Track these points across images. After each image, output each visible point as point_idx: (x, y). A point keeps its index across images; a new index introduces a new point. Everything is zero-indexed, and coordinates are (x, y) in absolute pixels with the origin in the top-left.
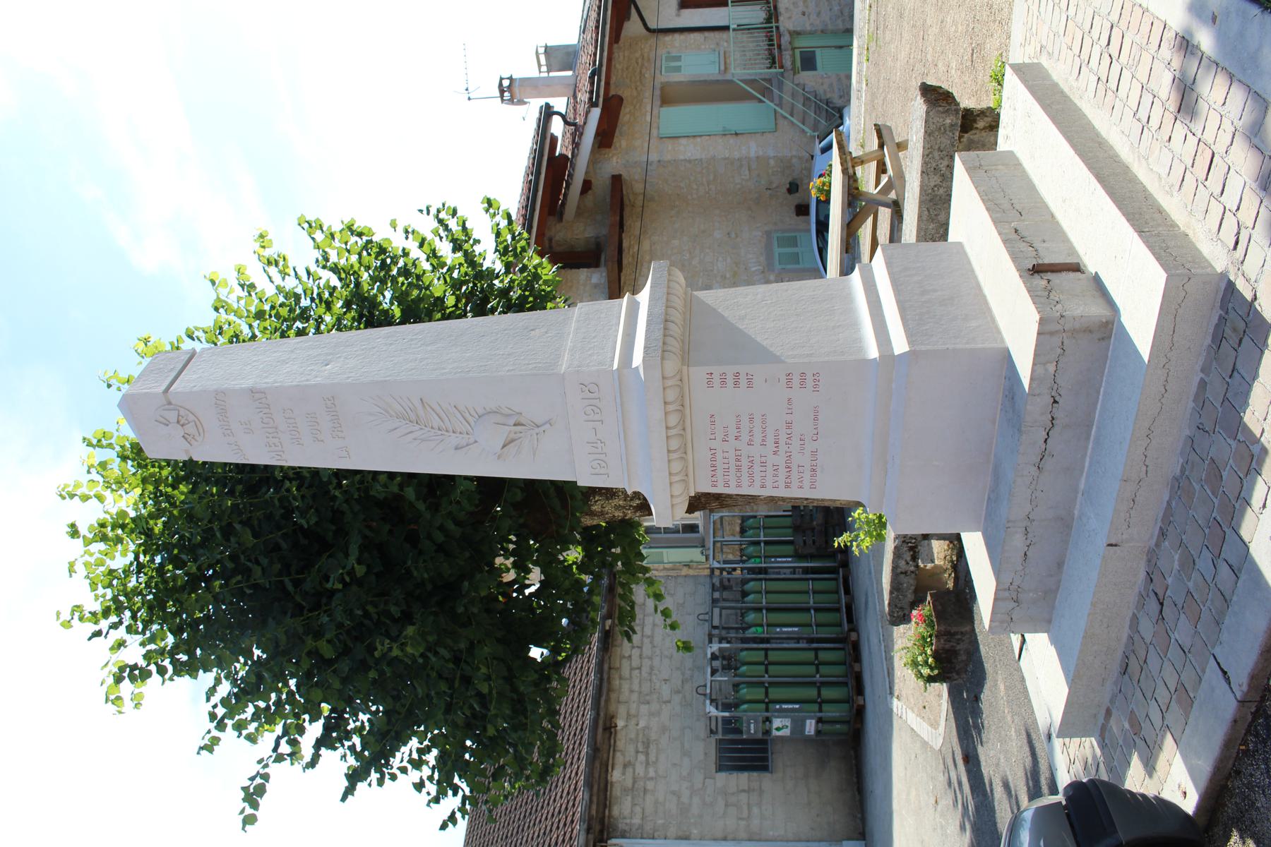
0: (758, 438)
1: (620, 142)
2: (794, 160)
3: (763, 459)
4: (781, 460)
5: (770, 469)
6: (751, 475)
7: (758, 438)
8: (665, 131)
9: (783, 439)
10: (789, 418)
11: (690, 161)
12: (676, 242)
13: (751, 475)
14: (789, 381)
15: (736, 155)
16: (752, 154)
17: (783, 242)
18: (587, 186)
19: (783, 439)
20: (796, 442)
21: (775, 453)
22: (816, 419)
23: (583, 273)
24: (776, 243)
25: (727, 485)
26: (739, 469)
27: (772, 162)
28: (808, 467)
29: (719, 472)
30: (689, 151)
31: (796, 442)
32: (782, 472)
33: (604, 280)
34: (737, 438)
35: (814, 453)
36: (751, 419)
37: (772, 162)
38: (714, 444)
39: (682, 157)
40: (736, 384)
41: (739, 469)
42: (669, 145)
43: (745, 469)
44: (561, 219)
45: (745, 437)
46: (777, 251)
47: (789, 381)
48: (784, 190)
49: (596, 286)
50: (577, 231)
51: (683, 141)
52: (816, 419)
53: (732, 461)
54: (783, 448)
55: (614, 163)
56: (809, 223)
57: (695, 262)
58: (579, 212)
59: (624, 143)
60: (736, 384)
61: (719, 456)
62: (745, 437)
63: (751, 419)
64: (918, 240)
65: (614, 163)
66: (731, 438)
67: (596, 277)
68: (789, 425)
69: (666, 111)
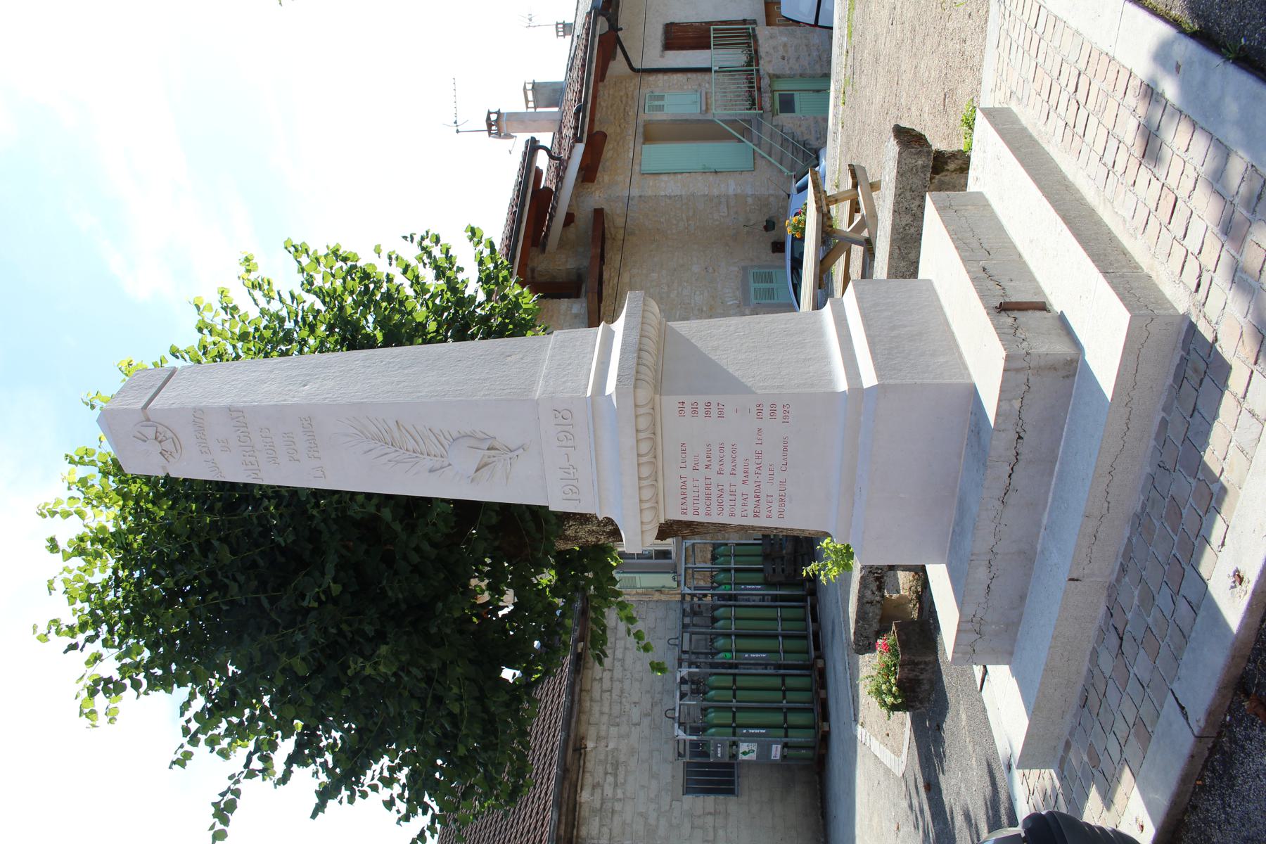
0: (727, 468)
1: (603, 177)
2: (771, 199)
3: (733, 488)
4: (750, 489)
5: (739, 498)
6: (720, 504)
7: (727, 468)
8: (646, 167)
9: (752, 468)
10: (759, 448)
11: (670, 197)
12: (655, 275)
13: (720, 504)
14: (759, 412)
15: (716, 192)
16: (731, 192)
17: (760, 278)
18: (570, 218)
19: (752, 468)
20: (765, 472)
21: (745, 482)
22: (785, 449)
23: (564, 303)
24: (752, 280)
25: (696, 512)
26: (708, 497)
27: (750, 200)
28: (776, 497)
29: (690, 501)
30: (670, 187)
31: (765, 472)
32: (751, 503)
33: (583, 311)
34: (707, 467)
35: (783, 483)
36: (722, 449)
37: (750, 200)
38: (684, 473)
39: (663, 193)
40: (707, 413)
41: (708, 497)
42: (651, 181)
43: (714, 498)
44: (543, 250)
45: (715, 466)
46: (753, 286)
47: (759, 412)
48: (762, 227)
49: (576, 316)
50: (558, 262)
51: (665, 178)
52: (785, 449)
53: (702, 489)
54: (752, 477)
55: (597, 197)
56: (784, 259)
57: (673, 295)
58: (562, 244)
59: (606, 178)
60: (707, 413)
61: (689, 483)
62: (715, 466)
63: (722, 449)
64: (889, 277)
65: (597, 197)
66: (702, 467)
67: (577, 307)
68: (759, 455)
69: (646, 147)
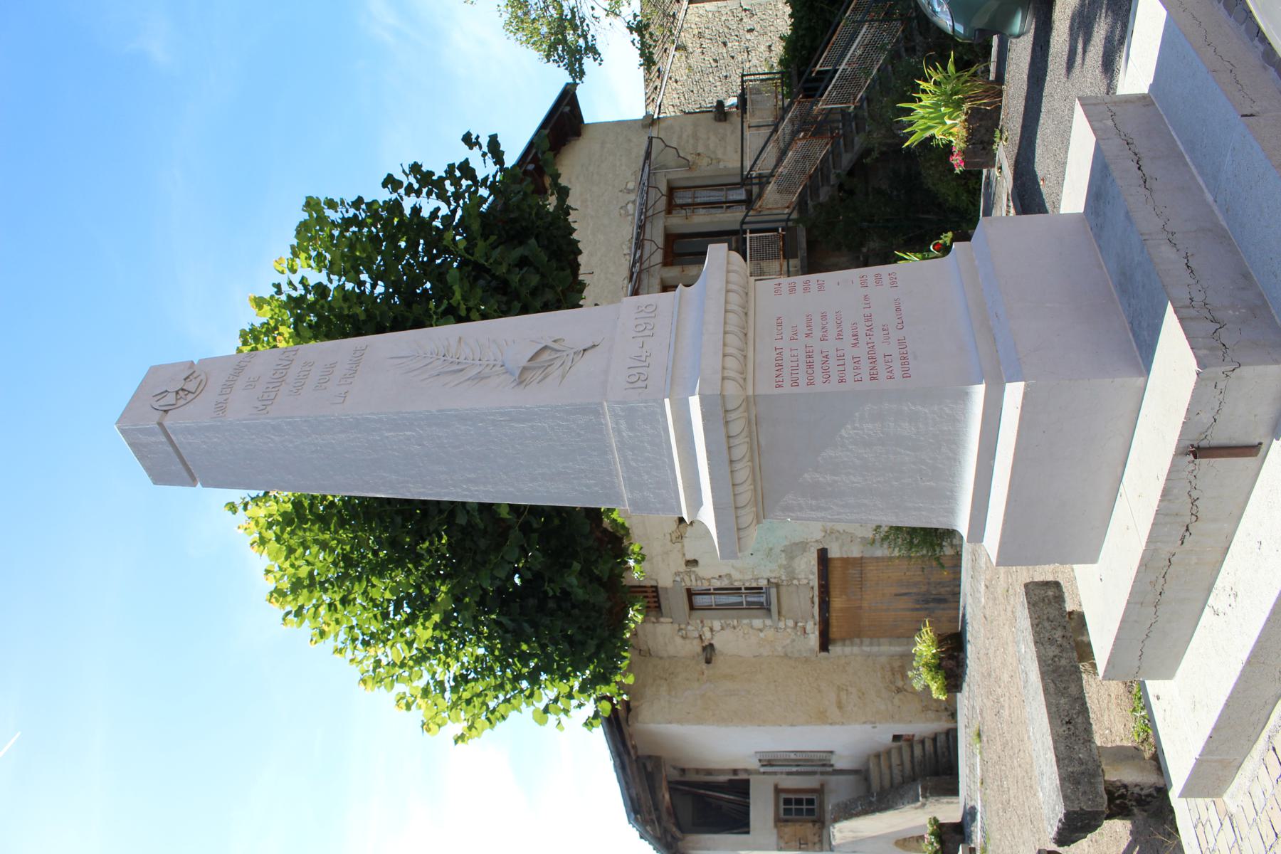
4: (862, 352)
5: (850, 365)
6: (826, 371)
7: (832, 332)
10: (867, 312)
13: (826, 371)
19: (862, 331)
25: (795, 383)
29: (786, 372)
35: (902, 342)
66: (801, 336)
68: (868, 318)
